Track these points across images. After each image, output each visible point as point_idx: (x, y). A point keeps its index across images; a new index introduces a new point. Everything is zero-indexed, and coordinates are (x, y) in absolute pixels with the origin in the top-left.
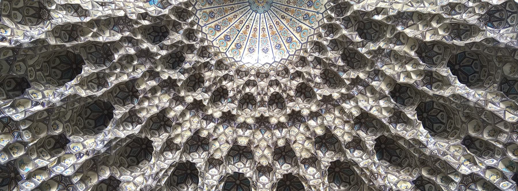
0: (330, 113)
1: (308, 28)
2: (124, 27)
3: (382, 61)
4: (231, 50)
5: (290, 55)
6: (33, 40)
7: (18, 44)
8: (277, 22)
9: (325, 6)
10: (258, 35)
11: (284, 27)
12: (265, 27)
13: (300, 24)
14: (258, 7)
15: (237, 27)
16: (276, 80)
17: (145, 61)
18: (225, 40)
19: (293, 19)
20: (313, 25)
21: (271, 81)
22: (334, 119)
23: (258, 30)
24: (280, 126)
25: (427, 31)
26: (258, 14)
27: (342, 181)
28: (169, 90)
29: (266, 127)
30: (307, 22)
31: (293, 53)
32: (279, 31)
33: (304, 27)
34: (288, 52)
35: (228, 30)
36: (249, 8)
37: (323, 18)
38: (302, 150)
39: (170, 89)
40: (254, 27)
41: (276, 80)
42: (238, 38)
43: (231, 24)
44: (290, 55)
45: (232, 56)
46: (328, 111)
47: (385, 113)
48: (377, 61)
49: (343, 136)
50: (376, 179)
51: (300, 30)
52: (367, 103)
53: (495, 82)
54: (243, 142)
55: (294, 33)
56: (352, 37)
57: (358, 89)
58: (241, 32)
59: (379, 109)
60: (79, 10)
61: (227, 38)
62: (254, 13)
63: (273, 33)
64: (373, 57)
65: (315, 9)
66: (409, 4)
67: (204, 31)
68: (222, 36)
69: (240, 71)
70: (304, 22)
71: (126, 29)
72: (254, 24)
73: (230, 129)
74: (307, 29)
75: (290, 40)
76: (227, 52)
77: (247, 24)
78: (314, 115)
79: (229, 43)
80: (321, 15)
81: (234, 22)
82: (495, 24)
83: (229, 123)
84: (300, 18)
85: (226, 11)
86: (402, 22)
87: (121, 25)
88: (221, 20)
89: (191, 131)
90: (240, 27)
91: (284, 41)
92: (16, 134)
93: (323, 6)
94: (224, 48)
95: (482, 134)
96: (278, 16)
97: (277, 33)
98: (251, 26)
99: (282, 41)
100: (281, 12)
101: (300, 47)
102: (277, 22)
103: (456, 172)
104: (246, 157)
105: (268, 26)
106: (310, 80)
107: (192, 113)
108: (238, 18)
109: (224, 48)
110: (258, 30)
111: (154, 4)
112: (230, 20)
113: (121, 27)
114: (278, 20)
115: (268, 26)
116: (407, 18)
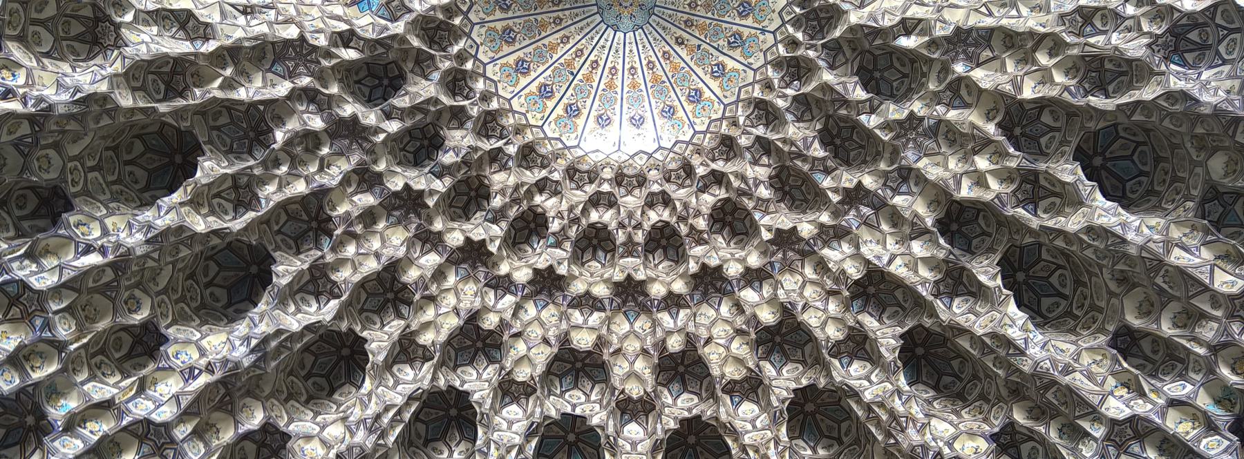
0: (792, 271)
1: (741, 67)
2: (297, 66)
3: (919, 147)
4: (556, 121)
5: (696, 132)
6: (79, 96)
7: (43, 105)
8: (664, 53)
9: (780, 14)
10: (619, 83)
11: (683, 64)
12: (637, 65)
13: (722, 58)
14: (619, 16)
15: (569, 64)
16: (663, 192)
17: (349, 148)
18: (541, 96)
19: (704, 46)
20: (751, 60)
21: (652, 194)
22: (803, 286)
23: (620, 73)
24: (673, 302)
25: (1026, 74)
26: (620, 35)
27: (822, 435)
28: (406, 216)
29: (638, 305)
30: (737, 54)
31: (704, 128)
32: (670, 75)
33: (730, 64)
34: (692, 125)
35: (549, 72)
36: (598, 18)
37: (775, 44)
38: (725, 360)
39: (407, 213)
40: (609, 65)
41: (663, 192)
42: (570, 91)
43: (555, 57)
44: (696, 132)
45: (556, 135)
46: (788, 267)
47: (924, 272)
48: (905, 146)
49: (823, 326)
50: (903, 430)
51: (719, 72)
52: (881, 248)
53: (1188, 198)
54: (583, 340)
55: (707, 79)
56: (845, 88)
57: (859, 215)
58: (579, 77)
59: (911, 262)
60: (191, 24)
61: (545, 92)
62: (610, 32)
63: (656, 80)
64: (897, 137)
65: (756, 21)
66: (983, 9)
67: (489, 74)
68: (533, 87)
69: (577, 170)
70: (730, 53)
71: (302, 69)
72: (611, 58)
73: (552, 309)
74: (737, 71)
75: (696, 97)
76: (545, 124)
77: (592, 58)
78: (753, 277)
79: (550, 104)
80: (770, 37)
81: (562, 53)
82: (1189, 57)
83: (551, 295)
84: (721, 42)
85: (543, 26)
86: (964, 52)
87: (290, 59)
88: (530, 49)
89: (458, 314)
90: (577, 66)
91: (683, 99)
92: (38, 322)
93: (776, 15)
94: (539, 116)
95: (1158, 321)
96: (668, 38)
97: (664, 78)
98: (602, 63)
99: (677, 98)
100: (674, 29)
101: (720, 112)
102: (664, 53)
103: (1094, 414)
104: (590, 378)
105: (644, 63)
106: (744, 193)
107: (462, 272)
108: (572, 42)
109: (539, 116)
110: (620, 73)
111: (370, 9)
112: (553, 48)
113: (291, 64)
114: (667, 48)
115: (644, 63)
116: (976, 44)
